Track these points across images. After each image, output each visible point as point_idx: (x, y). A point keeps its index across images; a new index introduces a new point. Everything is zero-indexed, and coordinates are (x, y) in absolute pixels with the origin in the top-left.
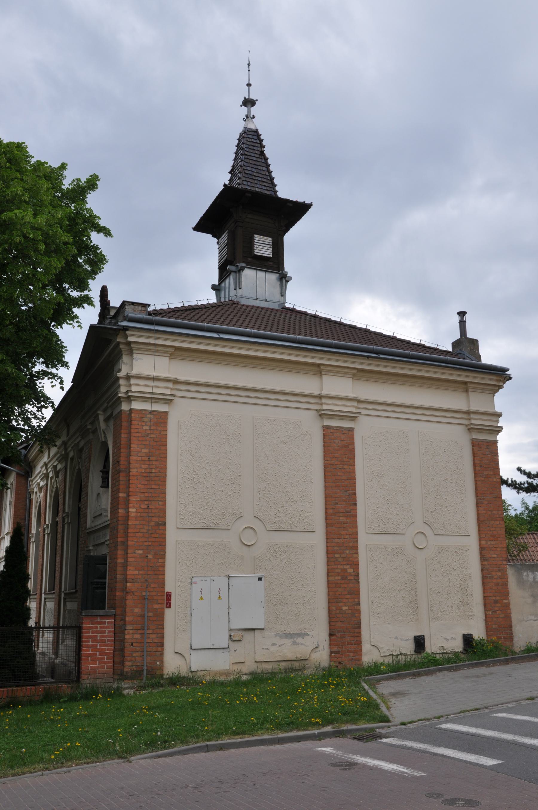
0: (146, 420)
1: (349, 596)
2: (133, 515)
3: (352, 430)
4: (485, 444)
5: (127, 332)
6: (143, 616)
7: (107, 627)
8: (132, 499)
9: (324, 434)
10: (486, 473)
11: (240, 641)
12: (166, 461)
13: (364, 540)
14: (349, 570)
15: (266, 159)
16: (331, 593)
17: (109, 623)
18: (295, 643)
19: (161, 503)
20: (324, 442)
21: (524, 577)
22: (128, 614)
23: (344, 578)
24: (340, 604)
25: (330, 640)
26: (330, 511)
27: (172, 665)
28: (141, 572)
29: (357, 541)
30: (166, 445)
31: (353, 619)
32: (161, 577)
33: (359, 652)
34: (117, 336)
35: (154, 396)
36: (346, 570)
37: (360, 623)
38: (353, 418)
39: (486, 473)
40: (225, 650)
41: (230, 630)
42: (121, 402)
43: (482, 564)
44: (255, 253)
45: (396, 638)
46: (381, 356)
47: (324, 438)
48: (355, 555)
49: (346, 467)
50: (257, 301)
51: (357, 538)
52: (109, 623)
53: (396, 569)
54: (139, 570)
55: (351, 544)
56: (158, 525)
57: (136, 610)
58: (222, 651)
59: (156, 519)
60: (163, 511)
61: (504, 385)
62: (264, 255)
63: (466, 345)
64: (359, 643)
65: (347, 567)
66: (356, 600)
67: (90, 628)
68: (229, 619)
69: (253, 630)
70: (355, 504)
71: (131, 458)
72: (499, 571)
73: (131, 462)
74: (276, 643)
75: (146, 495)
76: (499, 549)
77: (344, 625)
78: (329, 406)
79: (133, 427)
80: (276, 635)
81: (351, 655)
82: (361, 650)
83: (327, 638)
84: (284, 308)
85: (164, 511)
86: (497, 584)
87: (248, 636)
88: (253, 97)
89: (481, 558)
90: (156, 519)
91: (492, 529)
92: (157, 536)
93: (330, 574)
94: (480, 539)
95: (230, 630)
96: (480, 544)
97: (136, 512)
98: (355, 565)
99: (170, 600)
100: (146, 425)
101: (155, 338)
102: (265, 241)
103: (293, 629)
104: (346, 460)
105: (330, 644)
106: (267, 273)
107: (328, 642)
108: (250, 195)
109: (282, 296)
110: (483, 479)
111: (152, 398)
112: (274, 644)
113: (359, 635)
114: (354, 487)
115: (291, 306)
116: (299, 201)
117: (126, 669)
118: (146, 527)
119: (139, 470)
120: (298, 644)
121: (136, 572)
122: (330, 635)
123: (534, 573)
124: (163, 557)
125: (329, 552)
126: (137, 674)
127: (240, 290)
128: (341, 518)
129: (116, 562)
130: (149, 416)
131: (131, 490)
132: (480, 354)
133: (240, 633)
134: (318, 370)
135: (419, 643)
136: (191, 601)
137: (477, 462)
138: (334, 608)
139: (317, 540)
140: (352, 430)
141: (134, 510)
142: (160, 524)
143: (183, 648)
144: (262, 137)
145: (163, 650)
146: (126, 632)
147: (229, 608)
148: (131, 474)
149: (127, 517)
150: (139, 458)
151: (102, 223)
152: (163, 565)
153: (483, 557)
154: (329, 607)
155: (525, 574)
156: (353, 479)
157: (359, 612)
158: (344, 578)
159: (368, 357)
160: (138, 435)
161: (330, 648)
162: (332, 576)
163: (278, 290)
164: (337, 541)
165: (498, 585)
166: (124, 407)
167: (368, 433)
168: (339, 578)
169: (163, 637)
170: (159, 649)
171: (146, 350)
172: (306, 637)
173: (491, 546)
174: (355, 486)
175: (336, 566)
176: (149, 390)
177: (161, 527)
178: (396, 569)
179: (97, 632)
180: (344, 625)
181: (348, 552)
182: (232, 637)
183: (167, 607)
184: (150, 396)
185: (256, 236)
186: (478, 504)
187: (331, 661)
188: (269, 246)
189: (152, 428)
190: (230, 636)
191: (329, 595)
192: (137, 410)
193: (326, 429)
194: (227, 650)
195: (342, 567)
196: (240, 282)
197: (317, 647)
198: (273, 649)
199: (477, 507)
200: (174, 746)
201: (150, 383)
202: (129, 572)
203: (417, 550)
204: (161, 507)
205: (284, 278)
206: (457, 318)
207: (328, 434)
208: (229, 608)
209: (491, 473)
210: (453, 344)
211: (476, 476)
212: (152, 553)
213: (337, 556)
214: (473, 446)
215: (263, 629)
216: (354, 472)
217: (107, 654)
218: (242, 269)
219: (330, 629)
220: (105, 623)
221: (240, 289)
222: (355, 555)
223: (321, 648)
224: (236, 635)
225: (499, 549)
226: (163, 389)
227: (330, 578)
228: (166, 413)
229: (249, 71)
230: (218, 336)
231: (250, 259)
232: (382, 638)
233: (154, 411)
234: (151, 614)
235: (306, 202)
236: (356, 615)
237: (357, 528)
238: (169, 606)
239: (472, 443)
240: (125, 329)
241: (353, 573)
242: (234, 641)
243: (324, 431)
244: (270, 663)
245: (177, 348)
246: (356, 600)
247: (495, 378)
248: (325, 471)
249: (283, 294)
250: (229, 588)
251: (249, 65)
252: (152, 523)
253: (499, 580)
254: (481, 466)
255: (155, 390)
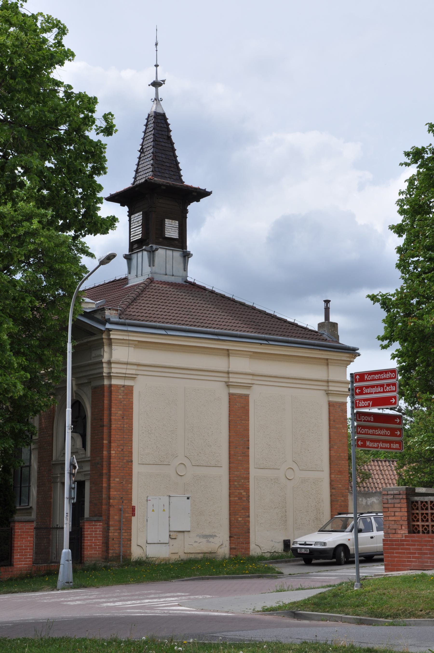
0: (120, 391)
1: (243, 511)
2: (113, 455)
3: (247, 396)
4: (338, 404)
5: (111, 332)
6: (120, 521)
7: (98, 528)
8: (113, 445)
9: (229, 399)
10: (337, 426)
11: (175, 539)
12: (132, 419)
13: (253, 472)
14: (243, 494)
15: (172, 144)
16: (231, 509)
17: (99, 525)
18: (208, 542)
19: (129, 447)
20: (229, 404)
21: (360, 502)
22: (111, 520)
23: (240, 498)
24: (237, 516)
25: (230, 540)
26: (232, 452)
27: (136, 553)
28: (118, 493)
29: (249, 473)
30: (132, 409)
31: (245, 527)
32: (130, 496)
33: (248, 549)
34: (102, 334)
35: (127, 375)
36: (241, 493)
37: (249, 529)
38: (248, 387)
39: (337, 426)
40: (167, 545)
41: (170, 531)
42: (104, 379)
43: (331, 492)
44: (166, 236)
45: (272, 541)
46: (271, 343)
47: (229, 402)
48: (247, 483)
49: (243, 422)
50: (166, 276)
51: (249, 471)
52: (99, 525)
53: (273, 493)
54: (117, 492)
55: (245, 475)
56: (128, 462)
57: (116, 517)
58: (165, 545)
59: (127, 458)
60: (131, 453)
61: (355, 360)
62: (172, 237)
63: (330, 327)
64: (248, 543)
65: (242, 491)
66: (247, 514)
67: (89, 528)
68: (169, 524)
69: (183, 532)
70: (248, 448)
71: (112, 417)
72: (343, 496)
73: (112, 420)
74: (197, 541)
75: (121, 442)
76: (343, 481)
77: (239, 530)
78: (233, 379)
79: (113, 396)
80: (197, 536)
81: (243, 550)
82: (249, 548)
83: (228, 539)
84: (186, 281)
85: (131, 453)
86: (341, 506)
87: (180, 536)
88: (160, 79)
89: (330, 487)
90: (127, 458)
91: (339, 467)
92: (127, 469)
93: (231, 496)
94: (331, 474)
95: (170, 531)
96: (330, 477)
97: (115, 453)
98: (247, 490)
99: (134, 511)
100: (121, 395)
101: (128, 336)
102: (174, 224)
103: (207, 532)
104: (243, 417)
105: (230, 543)
106: (174, 252)
107: (228, 542)
108: (164, 188)
109: (185, 271)
110: (335, 430)
111: (125, 377)
112: (196, 542)
113: (248, 537)
114: (248, 436)
115: (192, 280)
116: (201, 188)
117: (110, 555)
118: (121, 463)
119: (117, 426)
120: (210, 542)
121: (116, 493)
122: (230, 537)
123: (366, 499)
124: (131, 483)
125: (230, 481)
126: (117, 558)
127: (154, 267)
128: (239, 458)
129: (102, 487)
130: (123, 389)
131: (112, 439)
132: (339, 334)
133: (175, 533)
134: (228, 353)
135: (287, 544)
136: (147, 512)
137: (332, 418)
138: (233, 519)
139: (223, 472)
140: (247, 396)
141: (114, 452)
142: (129, 462)
143: (142, 542)
144: (169, 121)
145: (131, 543)
146: (110, 531)
147: (169, 517)
148: (112, 428)
149: (109, 457)
150: (117, 418)
151: (90, 251)
152: (131, 489)
153: (332, 487)
154: (230, 518)
155: (360, 499)
156: (248, 430)
157: (249, 522)
158: (240, 498)
159: (261, 344)
160: (116, 402)
161: (230, 545)
162: (232, 497)
163: (182, 266)
164: (236, 473)
165: (341, 506)
166: (106, 382)
167: (260, 399)
168: (237, 498)
169: (131, 535)
170: (129, 543)
171: (123, 343)
172: (215, 538)
173: (338, 479)
174: (249, 435)
175: (235, 491)
176: (124, 371)
177: (130, 464)
178: (273, 493)
179: (93, 531)
180: (239, 530)
181: (243, 481)
182: (171, 536)
183: (133, 516)
184: (124, 375)
185: (166, 220)
186: (331, 448)
187: (230, 554)
188: (176, 229)
189: (125, 397)
190: (170, 535)
191: (230, 510)
192: (117, 386)
193: (231, 396)
194: (168, 545)
195: (239, 491)
196: (153, 261)
197: (222, 545)
198: (195, 545)
199: (330, 450)
200: (183, 578)
201: (125, 366)
202: (111, 493)
203: (287, 480)
204: (130, 450)
205: (186, 255)
206: (323, 305)
207: (232, 398)
208: (169, 517)
209: (341, 426)
210: (319, 324)
211: (330, 428)
212: (125, 480)
213: (236, 483)
214: (329, 406)
215: (189, 531)
216: (248, 425)
217: (98, 545)
218: (157, 249)
219: (230, 533)
220: (97, 525)
221: (153, 266)
222: (247, 483)
223: (224, 545)
224: (173, 535)
225: (343, 481)
226: (131, 371)
227: (231, 499)
228: (132, 387)
229: (157, 51)
230: (166, 333)
231: (160, 240)
232: (264, 540)
233: (126, 385)
234: (124, 520)
235: (207, 190)
236: (247, 524)
237: (249, 464)
238: (134, 515)
239: (329, 404)
240: (109, 330)
241: (246, 496)
242: (172, 539)
243: (229, 396)
244: (193, 554)
245: (139, 341)
246: (247, 514)
247: (348, 355)
248: (229, 424)
249: (185, 269)
250: (169, 504)
251: (156, 45)
252: (125, 461)
253: (342, 503)
254: (334, 421)
255: (128, 372)
